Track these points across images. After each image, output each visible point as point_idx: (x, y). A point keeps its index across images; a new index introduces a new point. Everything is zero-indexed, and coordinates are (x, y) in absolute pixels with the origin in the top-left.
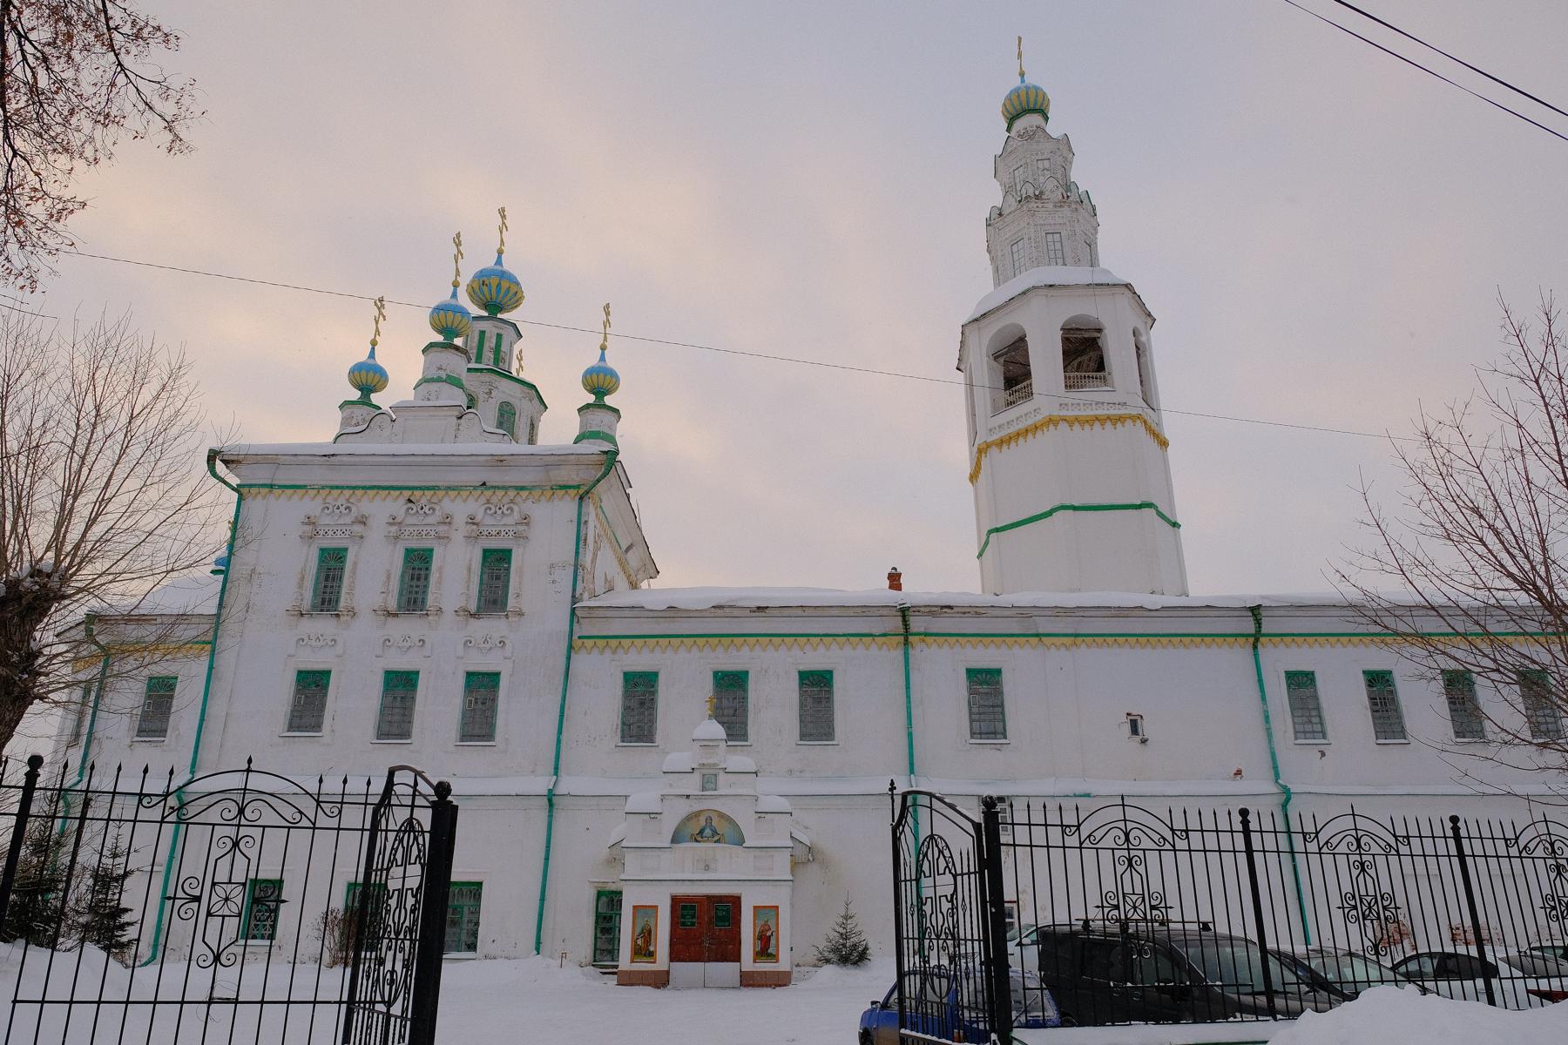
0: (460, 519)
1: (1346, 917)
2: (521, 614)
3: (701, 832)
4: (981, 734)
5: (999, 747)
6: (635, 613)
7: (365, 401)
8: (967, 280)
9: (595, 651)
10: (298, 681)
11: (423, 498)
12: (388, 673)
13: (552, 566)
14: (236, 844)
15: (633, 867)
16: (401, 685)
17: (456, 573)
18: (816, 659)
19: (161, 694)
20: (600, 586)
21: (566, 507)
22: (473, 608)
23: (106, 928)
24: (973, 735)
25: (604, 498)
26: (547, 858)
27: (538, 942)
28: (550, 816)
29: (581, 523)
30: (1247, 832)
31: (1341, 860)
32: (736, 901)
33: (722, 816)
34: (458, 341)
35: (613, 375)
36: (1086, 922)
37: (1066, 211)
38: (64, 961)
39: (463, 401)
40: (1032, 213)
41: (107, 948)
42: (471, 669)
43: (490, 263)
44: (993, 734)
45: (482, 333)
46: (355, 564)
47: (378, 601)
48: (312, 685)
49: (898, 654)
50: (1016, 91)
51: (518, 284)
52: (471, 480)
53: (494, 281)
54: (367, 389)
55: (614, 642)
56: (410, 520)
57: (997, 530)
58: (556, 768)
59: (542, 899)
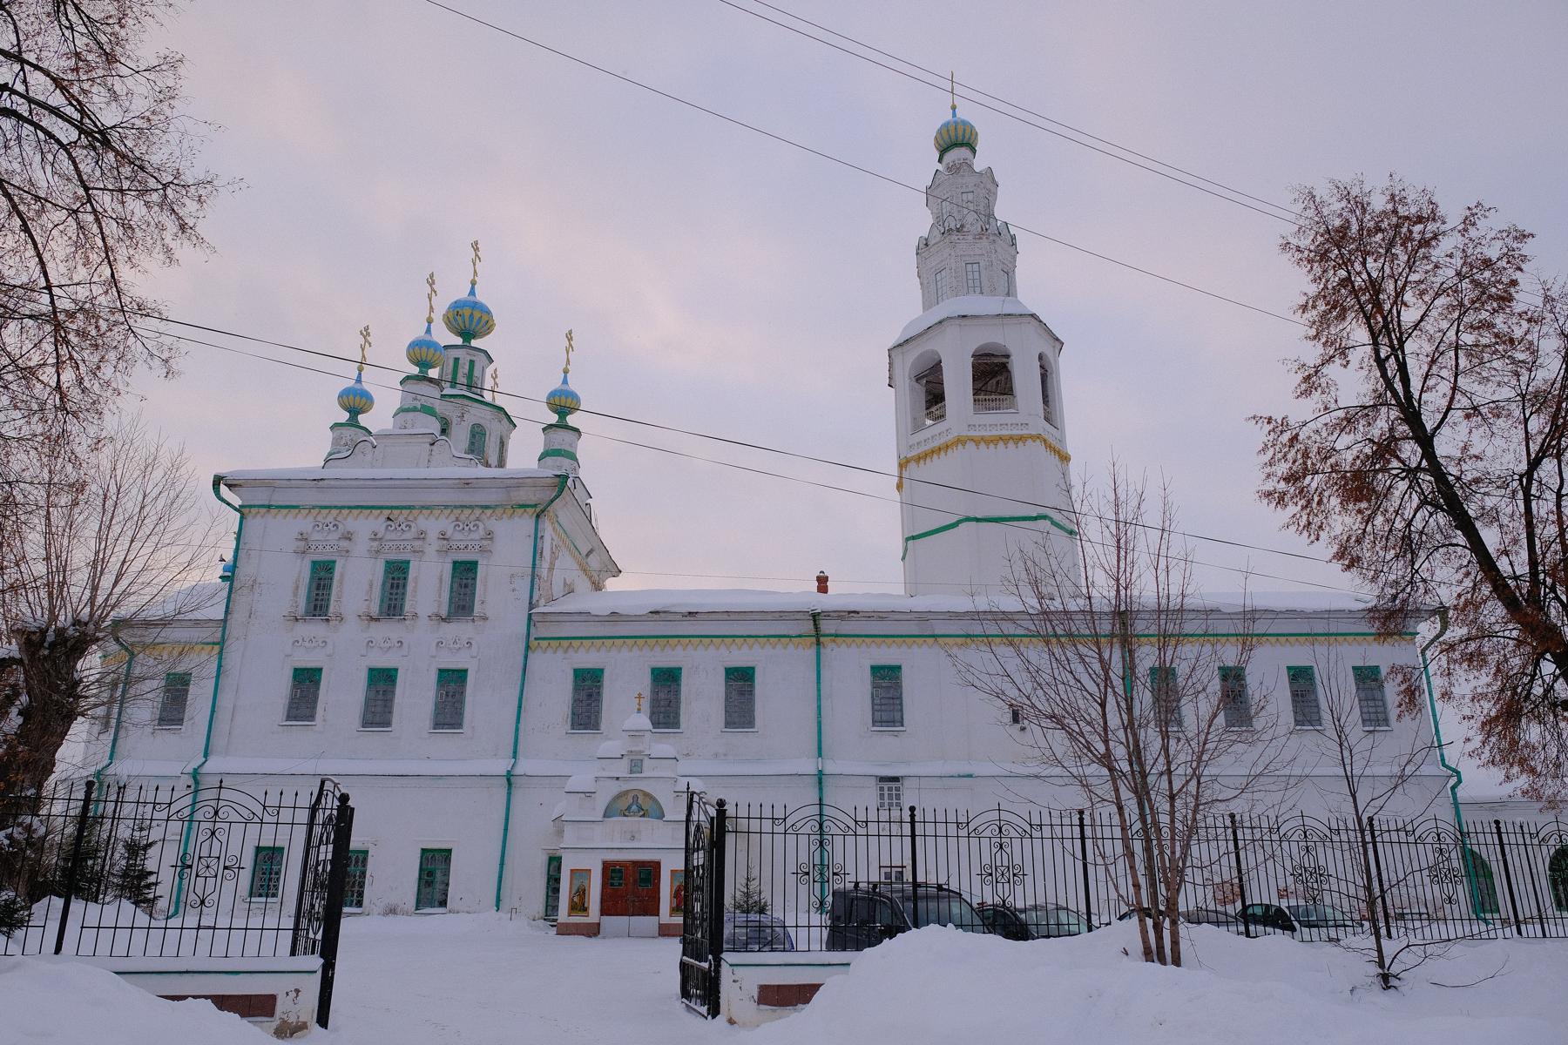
0: (433, 535)
1: (983, 881)
2: (485, 619)
3: (629, 808)
4: (882, 722)
5: (896, 734)
6: (583, 618)
7: (353, 422)
8: (901, 304)
9: (550, 651)
10: (295, 677)
11: (400, 516)
12: (371, 670)
14: (213, 833)
15: (570, 839)
16: (382, 681)
17: (429, 585)
18: (740, 657)
19: (177, 689)
20: (558, 589)
21: (525, 523)
22: (444, 613)
23: (136, 887)
24: (874, 723)
25: (560, 514)
26: (506, 829)
27: (498, 900)
28: (509, 794)
29: (537, 538)
30: (913, 823)
31: (985, 842)
32: (657, 865)
33: (646, 795)
34: (434, 373)
35: (574, 396)
36: (857, 884)
37: (985, 242)
38: (110, 910)
39: (435, 427)
40: (953, 244)
41: (136, 903)
42: (443, 666)
43: (463, 294)
44: (892, 722)
45: (457, 360)
46: (342, 575)
48: (306, 681)
49: (812, 652)
50: (946, 125)
51: (489, 313)
52: (449, 492)
53: (467, 312)
54: (354, 412)
55: (565, 643)
56: (388, 537)
57: (913, 538)
58: (515, 752)
59: (502, 864)
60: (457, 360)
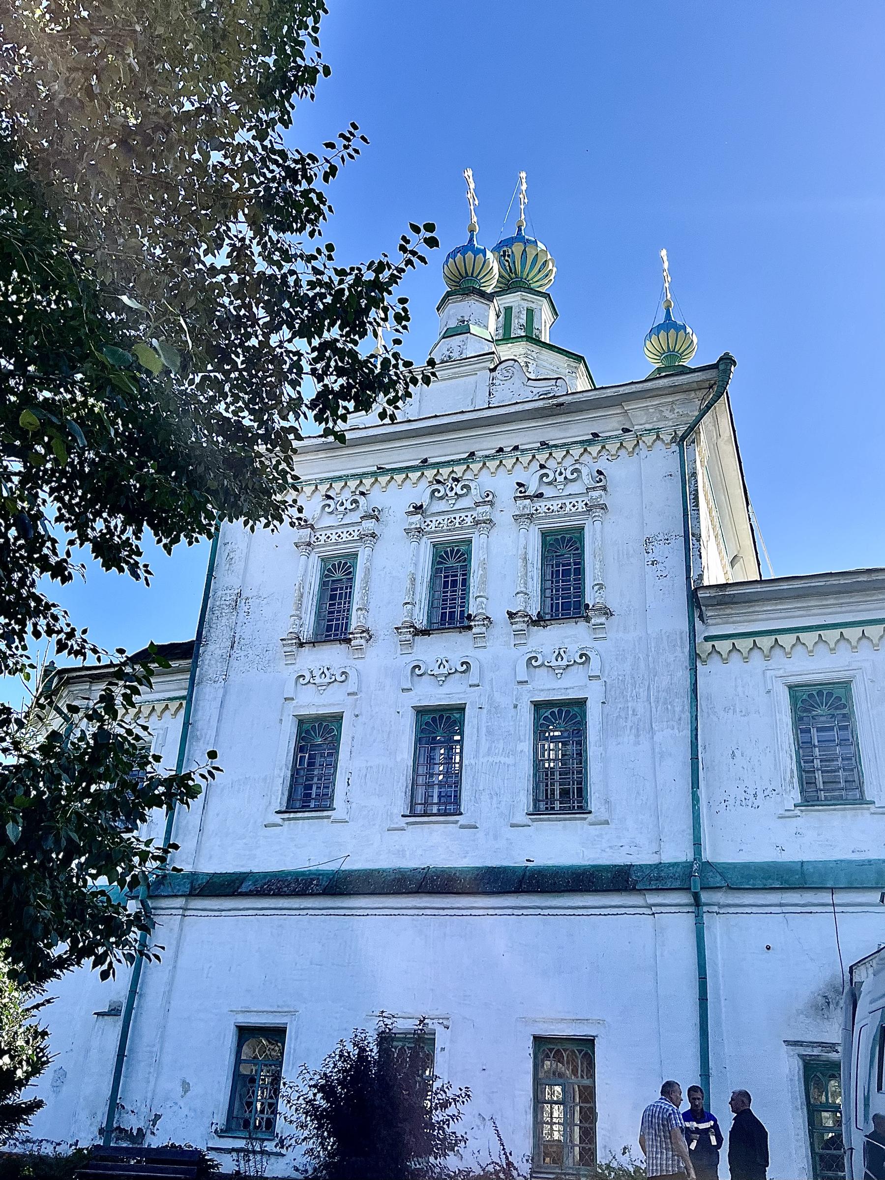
2: (607, 612)
13: (648, 541)
16: (439, 727)
17: (507, 567)
46: (368, 571)
47: (402, 617)
60: (508, 310)
